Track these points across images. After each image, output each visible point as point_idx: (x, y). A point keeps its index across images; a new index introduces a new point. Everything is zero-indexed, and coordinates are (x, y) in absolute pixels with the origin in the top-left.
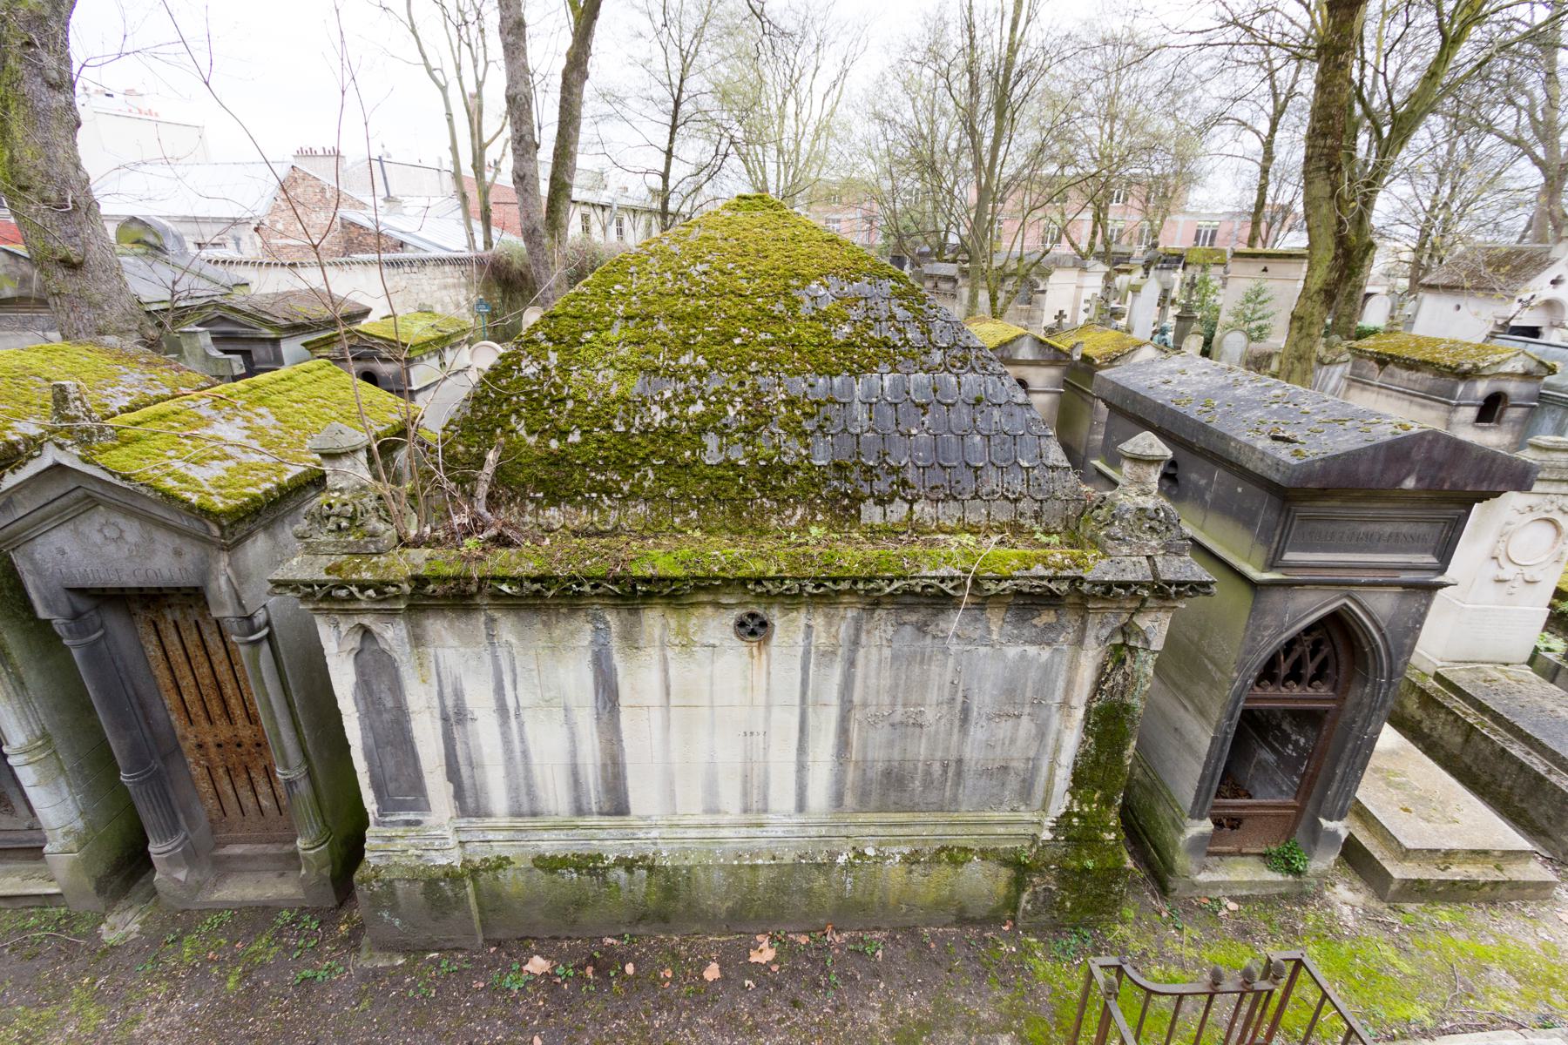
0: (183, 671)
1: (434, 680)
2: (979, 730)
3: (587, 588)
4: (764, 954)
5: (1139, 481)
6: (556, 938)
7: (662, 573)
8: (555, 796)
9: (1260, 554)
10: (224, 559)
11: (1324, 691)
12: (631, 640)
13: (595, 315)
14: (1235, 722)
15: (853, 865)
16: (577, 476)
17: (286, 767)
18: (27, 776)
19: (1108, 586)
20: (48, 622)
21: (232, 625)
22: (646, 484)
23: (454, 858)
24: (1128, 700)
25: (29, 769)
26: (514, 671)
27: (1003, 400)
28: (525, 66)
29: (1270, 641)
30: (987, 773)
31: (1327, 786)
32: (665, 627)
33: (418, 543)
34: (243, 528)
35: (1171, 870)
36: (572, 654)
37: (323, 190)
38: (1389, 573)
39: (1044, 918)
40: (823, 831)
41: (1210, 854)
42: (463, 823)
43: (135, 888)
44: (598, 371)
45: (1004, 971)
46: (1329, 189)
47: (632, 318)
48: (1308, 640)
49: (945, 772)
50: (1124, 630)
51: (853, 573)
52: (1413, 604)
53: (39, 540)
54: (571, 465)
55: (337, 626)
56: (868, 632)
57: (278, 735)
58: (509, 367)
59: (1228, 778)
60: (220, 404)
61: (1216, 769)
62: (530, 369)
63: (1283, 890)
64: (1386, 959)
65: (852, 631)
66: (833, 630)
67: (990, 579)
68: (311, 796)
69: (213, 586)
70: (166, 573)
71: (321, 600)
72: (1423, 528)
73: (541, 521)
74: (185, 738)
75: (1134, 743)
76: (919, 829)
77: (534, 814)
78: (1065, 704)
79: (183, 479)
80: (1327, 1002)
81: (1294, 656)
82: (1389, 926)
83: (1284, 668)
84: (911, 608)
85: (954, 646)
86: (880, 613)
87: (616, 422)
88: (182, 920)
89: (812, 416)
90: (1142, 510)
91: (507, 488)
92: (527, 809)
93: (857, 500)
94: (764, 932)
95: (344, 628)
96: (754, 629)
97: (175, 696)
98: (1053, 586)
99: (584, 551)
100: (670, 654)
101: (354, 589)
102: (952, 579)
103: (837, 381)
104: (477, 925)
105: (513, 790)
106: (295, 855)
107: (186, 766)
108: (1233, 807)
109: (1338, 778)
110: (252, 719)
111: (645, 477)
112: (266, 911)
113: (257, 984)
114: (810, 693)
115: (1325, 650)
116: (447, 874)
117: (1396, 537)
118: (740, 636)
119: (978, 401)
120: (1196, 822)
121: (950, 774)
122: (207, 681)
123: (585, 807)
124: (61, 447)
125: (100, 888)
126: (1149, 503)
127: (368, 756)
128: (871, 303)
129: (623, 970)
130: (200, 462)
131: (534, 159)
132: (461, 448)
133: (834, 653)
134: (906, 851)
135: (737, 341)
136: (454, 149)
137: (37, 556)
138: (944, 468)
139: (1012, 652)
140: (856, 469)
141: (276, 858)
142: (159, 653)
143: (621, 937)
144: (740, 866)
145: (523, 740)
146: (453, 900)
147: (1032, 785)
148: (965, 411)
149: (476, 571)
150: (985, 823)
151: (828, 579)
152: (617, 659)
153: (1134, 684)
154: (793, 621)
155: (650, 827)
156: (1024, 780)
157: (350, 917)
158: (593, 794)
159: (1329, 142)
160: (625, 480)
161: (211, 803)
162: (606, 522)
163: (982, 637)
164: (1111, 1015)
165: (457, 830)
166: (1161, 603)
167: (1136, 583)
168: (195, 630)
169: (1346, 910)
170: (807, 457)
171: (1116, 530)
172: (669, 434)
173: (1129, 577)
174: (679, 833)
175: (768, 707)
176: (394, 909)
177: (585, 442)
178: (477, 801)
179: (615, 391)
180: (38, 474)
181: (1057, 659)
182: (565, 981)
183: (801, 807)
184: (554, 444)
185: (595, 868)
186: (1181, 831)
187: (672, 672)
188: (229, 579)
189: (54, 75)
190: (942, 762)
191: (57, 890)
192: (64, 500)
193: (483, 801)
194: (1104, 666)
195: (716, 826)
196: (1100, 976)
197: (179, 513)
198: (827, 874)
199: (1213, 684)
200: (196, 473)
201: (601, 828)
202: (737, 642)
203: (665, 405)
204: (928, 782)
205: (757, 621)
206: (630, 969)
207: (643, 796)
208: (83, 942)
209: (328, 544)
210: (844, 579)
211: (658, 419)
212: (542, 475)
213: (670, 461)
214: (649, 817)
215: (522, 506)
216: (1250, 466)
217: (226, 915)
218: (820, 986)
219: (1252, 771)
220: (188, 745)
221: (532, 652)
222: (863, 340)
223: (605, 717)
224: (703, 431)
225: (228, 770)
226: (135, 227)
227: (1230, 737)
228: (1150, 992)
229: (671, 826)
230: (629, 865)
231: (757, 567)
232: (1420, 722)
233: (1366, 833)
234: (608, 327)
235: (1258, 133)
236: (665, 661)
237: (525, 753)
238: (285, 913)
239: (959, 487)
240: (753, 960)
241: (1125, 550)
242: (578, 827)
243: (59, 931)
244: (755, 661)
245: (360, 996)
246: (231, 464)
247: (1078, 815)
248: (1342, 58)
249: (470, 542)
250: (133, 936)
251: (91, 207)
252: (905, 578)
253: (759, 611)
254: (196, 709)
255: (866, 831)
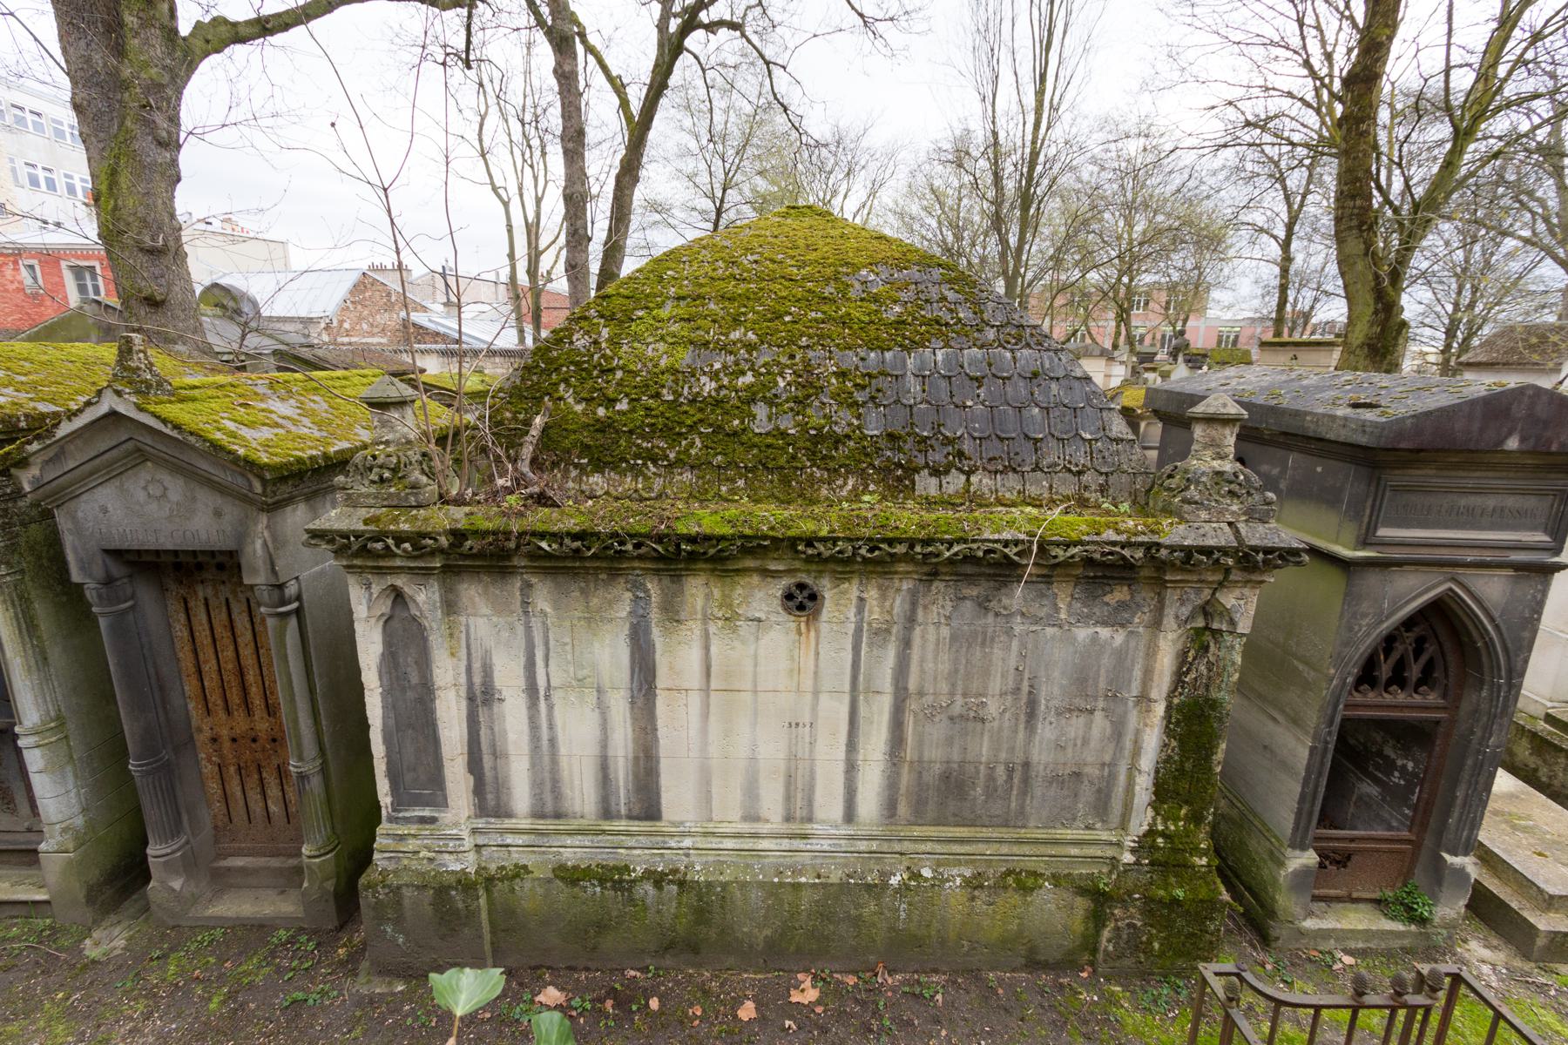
0: (207, 654)
1: (464, 651)
2: (1048, 727)
3: (629, 547)
4: (807, 993)
5: (1213, 444)
6: (572, 968)
7: (708, 531)
8: (582, 794)
9: (1350, 531)
10: (263, 519)
11: (1433, 698)
12: (672, 614)
13: (647, 296)
14: (1335, 728)
15: (908, 888)
16: (623, 443)
17: (300, 758)
18: (35, 760)
19: (1188, 551)
20: (80, 586)
21: (264, 594)
22: (693, 452)
23: (467, 864)
24: (1214, 694)
25: (37, 752)
26: (547, 644)
27: (1061, 374)
28: (582, 169)
29: (1369, 634)
30: (1055, 779)
31: (1447, 814)
32: (708, 597)
33: (459, 502)
34: (285, 490)
35: (1272, 914)
36: (608, 627)
37: (389, 295)
38: (1497, 553)
39: (1128, 962)
40: (874, 846)
41: (1316, 898)
42: (480, 823)
43: (126, 904)
44: (648, 345)
45: (1086, 1022)
46: (1362, 246)
47: (684, 298)
48: (1410, 637)
49: (1010, 777)
50: (1207, 610)
51: (910, 534)
52: (1528, 590)
53: (84, 497)
54: (617, 432)
55: (369, 587)
56: (925, 607)
57: (296, 721)
58: (561, 340)
59: (1331, 802)
60: (276, 386)
61: (1316, 787)
62: (580, 341)
63: (1406, 942)
64: (1547, 1025)
65: (907, 607)
66: (887, 604)
67: (1058, 544)
68: (323, 795)
69: (248, 549)
70: (204, 536)
71: (356, 555)
72: (1531, 502)
73: (584, 487)
74: (200, 730)
75: (1223, 746)
76: (981, 848)
77: (558, 815)
78: (1144, 699)
79: (233, 435)
80: (1502, 1024)
81: (1395, 656)
82: (1542, 989)
83: (1385, 671)
84: (970, 579)
85: (1019, 627)
86: (938, 585)
87: (665, 391)
88: (174, 933)
89: (863, 387)
90: (1219, 473)
91: (552, 453)
92: (550, 808)
93: (911, 470)
94: (807, 971)
95: (376, 589)
96: (802, 602)
97: (195, 682)
98: (1126, 553)
99: (628, 509)
100: (712, 629)
101: (390, 541)
102: (1017, 543)
103: (888, 355)
104: (487, 947)
105: (537, 785)
106: (298, 871)
107: (198, 762)
108: (1338, 839)
109: (1459, 802)
110: (271, 710)
111: (692, 444)
112: (261, 928)
113: (242, 1006)
114: (861, 678)
115: (1430, 649)
116: (459, 881)
117: (1500, 511)
118: (788, 610)
119: (1035, 375)
120: (1297, 852)
121: (1016, 781)
122: (230, 666)
123: (613, 807)
124: (119, 393)
125: (90, 899)
126: (1228, 466)
127: (387, 740)
128: (921, 287)
129: (647, 1005)
130: (251, 425)
131: (586, 251)
132: (508, 415)
133: (888, 631)
134: (968, 873)
135: (787, 319)
136: (511, 256)
137: (80, 514)
138: (1001, 439)
139: (1083, 633)
140: (910, 440)
141: (279, 872)
142: (186, 634)
143: (645, 970)
144: (781, 884)
145: (551, 727)
146: (463, 913)
147: (1108, 796)
148: (1021, 384)
149: (515, 526)
150: (1056, 842)
151: (884, 540)
152: (656, 633)
153: (1219, 675)
154: (844, 593)
155: (683, 835)
156: (1099, 791)
157: (350, 940)
158: (622, 792)
159: (1358, 203)
160: (671, 447)
161: (218, 806)
162: (651, 490)
163: (1049, 616)
164: (1234, 1024)
165: (474, 831)
166: (1247, 576)
167: (1219, 549)
168: (224, 609)
169: (1486, 969)
170: (859, 427)
171: (1193, 492)
172: (718, 403)
173: (1211, 542)
174: (714, 843)
175: (816, 693)
176: (398, 922)
177: (633, 410)
178: (498, 798)
179: (664, 362)
180: (93, 423)
181: (1132, 644)
182: (580, 1015)
183: (850, 816)
184: (601, 412)
185: (621, 881)
186: (1281, 864)
187: (713, 649)
188: (265, 543)
189: (164, 134)
190: (1007, 764)
191: (41, 896)
192: (114, 453)
193: (504, 798)
194: (1185, 653)
195: (755, 836)
196: (1217, 985)
197: (224, 468)
198: (878, 897)
199: (1306, 686)
200: (244, 432)
201: (629, 834)
202: (783, 616)
203: (715, 376)
204: (991, 791)
205: (806, 593)
206: (654, 1004)
207: (678, 799)
208: (63, 956)
209: (368, 496)
210: (900, 541)
211: (707, 389)
212: (588, 441)
213: (718, 429)
214: (682, 823)
215: (567, 471)
216: (1331, 436)
217: (218, 932)
218: (871, 1031)
219: (1352, 810)
220: (202, 738)
221: (567, 624)
222: (915, 319)
223: (640, 702)
224: (752, 400)
225: (240, 768)
226: (216, 291)
227: (1331, 747)
228: (1280, 1003)
229: (706, 834)
230: (658, 880)
231: (808, 527)
232: (1536, 770)
233: (1496, 881)
234: (659, 306)
235: (1275, 238)
236: (706, 637)
237: (553, 742)
238: (282, 932)
239: (1019, 459)
240: (794, 999)
241: (1204, 515)
242: (604, 831)
243: (40, 943)
244: (803, 638)
245: (353, 1023)
246: (281, 431)
247: (1163, 834)
248: (1363, 127)
249: (512, 499)
250: (119, 952)
251: (180, 256)
252: (965, 541)
253: (809, 581)
254: (215, 698)
255: (922, 847)
